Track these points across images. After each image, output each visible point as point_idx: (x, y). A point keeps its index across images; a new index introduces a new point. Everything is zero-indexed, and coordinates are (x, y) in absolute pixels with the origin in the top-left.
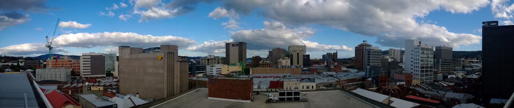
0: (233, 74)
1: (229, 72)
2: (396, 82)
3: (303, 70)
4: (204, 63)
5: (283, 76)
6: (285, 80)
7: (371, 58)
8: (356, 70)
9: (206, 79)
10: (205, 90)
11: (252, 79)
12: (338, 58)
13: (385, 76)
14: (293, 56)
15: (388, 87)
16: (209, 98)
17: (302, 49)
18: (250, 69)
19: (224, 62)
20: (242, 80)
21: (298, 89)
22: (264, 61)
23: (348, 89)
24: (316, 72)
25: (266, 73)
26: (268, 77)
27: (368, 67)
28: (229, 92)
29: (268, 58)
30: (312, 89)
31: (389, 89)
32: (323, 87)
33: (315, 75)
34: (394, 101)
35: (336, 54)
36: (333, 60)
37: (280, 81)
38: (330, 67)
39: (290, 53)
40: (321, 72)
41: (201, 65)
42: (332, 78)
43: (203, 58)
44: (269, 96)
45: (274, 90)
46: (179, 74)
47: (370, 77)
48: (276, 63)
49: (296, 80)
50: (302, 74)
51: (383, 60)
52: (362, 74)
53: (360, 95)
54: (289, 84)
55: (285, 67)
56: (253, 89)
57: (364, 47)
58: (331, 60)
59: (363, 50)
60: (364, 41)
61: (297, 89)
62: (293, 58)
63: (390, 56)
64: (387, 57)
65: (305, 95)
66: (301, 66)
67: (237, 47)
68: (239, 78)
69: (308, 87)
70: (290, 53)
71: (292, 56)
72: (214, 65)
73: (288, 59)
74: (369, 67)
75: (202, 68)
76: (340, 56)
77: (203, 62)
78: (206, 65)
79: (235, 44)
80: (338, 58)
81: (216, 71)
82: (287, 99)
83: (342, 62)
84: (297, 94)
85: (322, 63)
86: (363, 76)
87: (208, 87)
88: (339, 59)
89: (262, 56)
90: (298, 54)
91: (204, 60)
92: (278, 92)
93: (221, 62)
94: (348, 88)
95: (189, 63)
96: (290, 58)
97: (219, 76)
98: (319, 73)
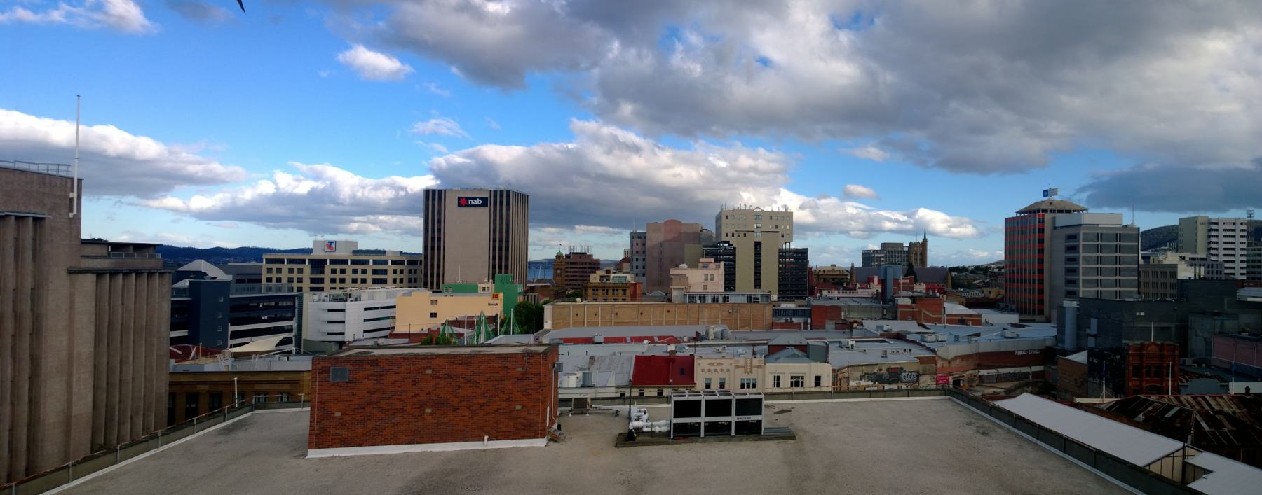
0: (457, 330)
1: (435, 324)
2: (1222, 380)
3: (777, 312)
4: (291, 280)
5: (694, 336)
6: (699, 352)
7: (1082, 266)
8: (1015, 318)
9: (303, 364)
10: (297, 418)
11: (553, 348)
12: (929, 266)
13: (1161, 347)
14: (734, 255)
15: (1178, 399)
16: (314, 454)
17: (777, 227)
18: (542, 310)
19: (413, 276)
20: (500, 356)
21: (754, 386)
22: (608, 272)
23: (979, 392)
24: (831, 319)
25: (617, 324)
26: (626, 342)
27: (1067, 303)
28: (432, 414)
29: (625, 260)
30: (817, 389)
31: (1181, 411)
32: (864, 383)
33: (829, 334)
34: (1209, 472)
35: (920, 250)
36: (910, 272)
37: (678, 354)
38: (892, 300)
39: (725, 242)
40: (855, 322)
41: (270, 289)
42: (900, 345)
43: (286, 257)
44: (630, 419)
45: (650, 392)
46: (85, 347)
47: (1079, 350)
48: (663, 282)
49: (749, 350)
50: (772, 326)
51: (1146, 273)
52: (1041, 333)
53: (1033, 425)
54: (719, 368)
55: (702, 297)
56: (560, 391)
57: (1048, 216)
58: (898, 272)
59: (1041, 231)
60: (1046, 193)
61: (751, 390)
62: (735, 261)
63: (1188, 255)
64: (1171, 258)
65: (785, 414)
66: (768, 296)
67: (486, 210)
68: (490, 345)
69: (797, 382)
70: (725, 242)
71: (732, 252)
72: (355, 290)
73: (713, 266)
74: (1074, 304)
75: (272, 308)
76: (938, 257)
77: (285, 276)
78: (300, 289)
79: (476, 198)
80: (929, 266)
81: (365, 320)
82: (705, 427)
83: (945, 279)
84: (751, 406)
85: (858, 286)
86: (1044, 340)
87: (306, 403)
88: (933, 269)
89: (598, 254)
90: (758, 244)
91: (349, 268)
92: (669, 402)
93: (398, 276)
94: (978, 388)
95: (174, 282)
96: (722, 263)
97: (380, 341)
98: (846, 326)
